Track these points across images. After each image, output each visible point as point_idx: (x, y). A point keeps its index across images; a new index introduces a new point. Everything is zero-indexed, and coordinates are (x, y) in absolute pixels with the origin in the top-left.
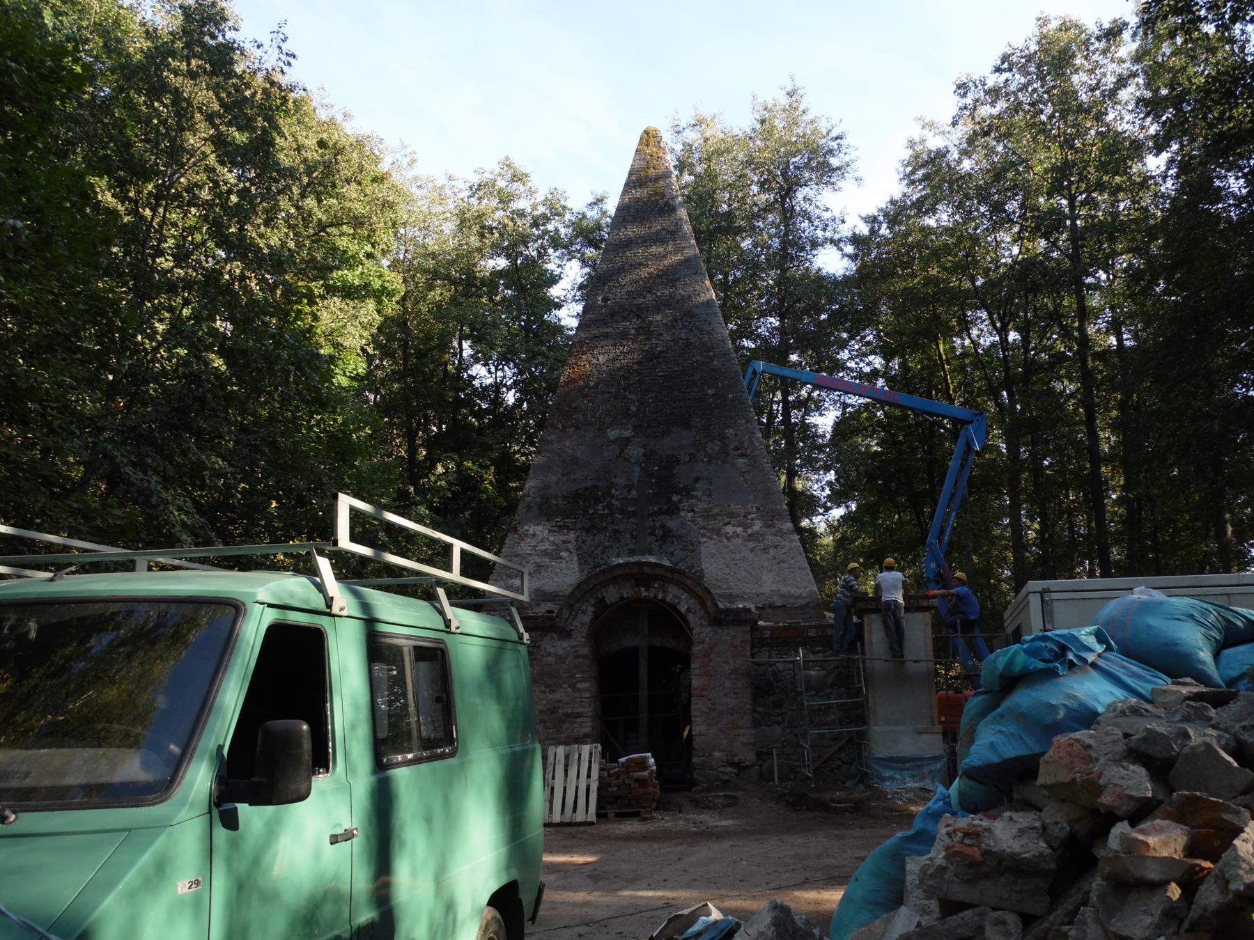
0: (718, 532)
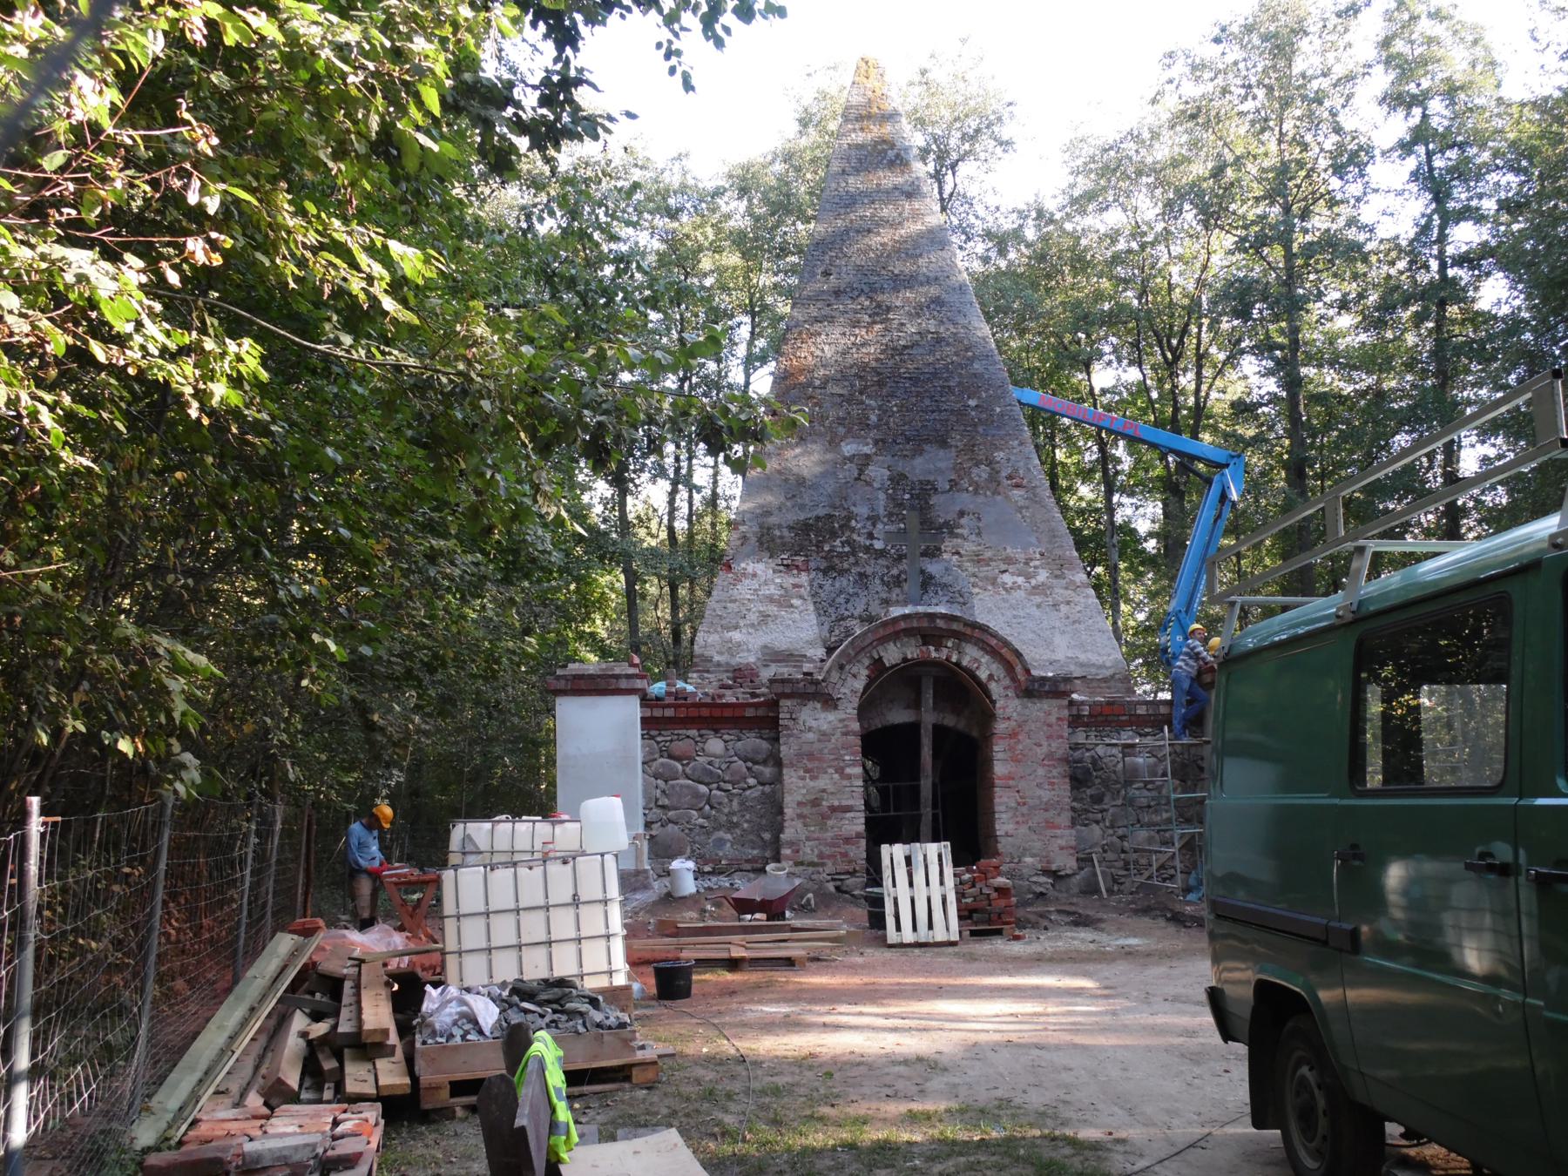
0: (994, 582)
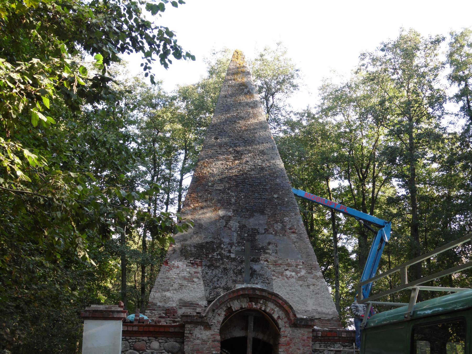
0: (282, 274)
